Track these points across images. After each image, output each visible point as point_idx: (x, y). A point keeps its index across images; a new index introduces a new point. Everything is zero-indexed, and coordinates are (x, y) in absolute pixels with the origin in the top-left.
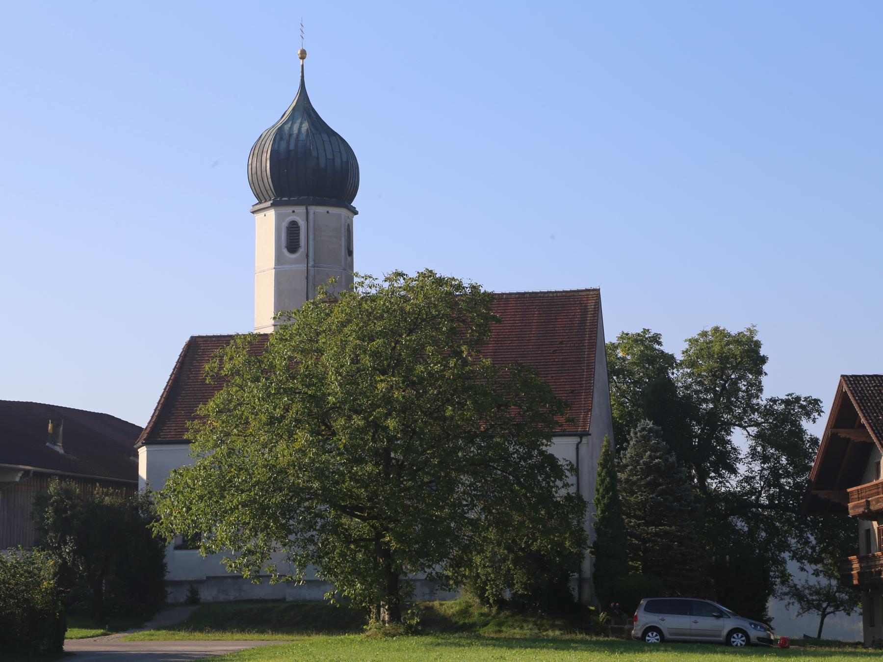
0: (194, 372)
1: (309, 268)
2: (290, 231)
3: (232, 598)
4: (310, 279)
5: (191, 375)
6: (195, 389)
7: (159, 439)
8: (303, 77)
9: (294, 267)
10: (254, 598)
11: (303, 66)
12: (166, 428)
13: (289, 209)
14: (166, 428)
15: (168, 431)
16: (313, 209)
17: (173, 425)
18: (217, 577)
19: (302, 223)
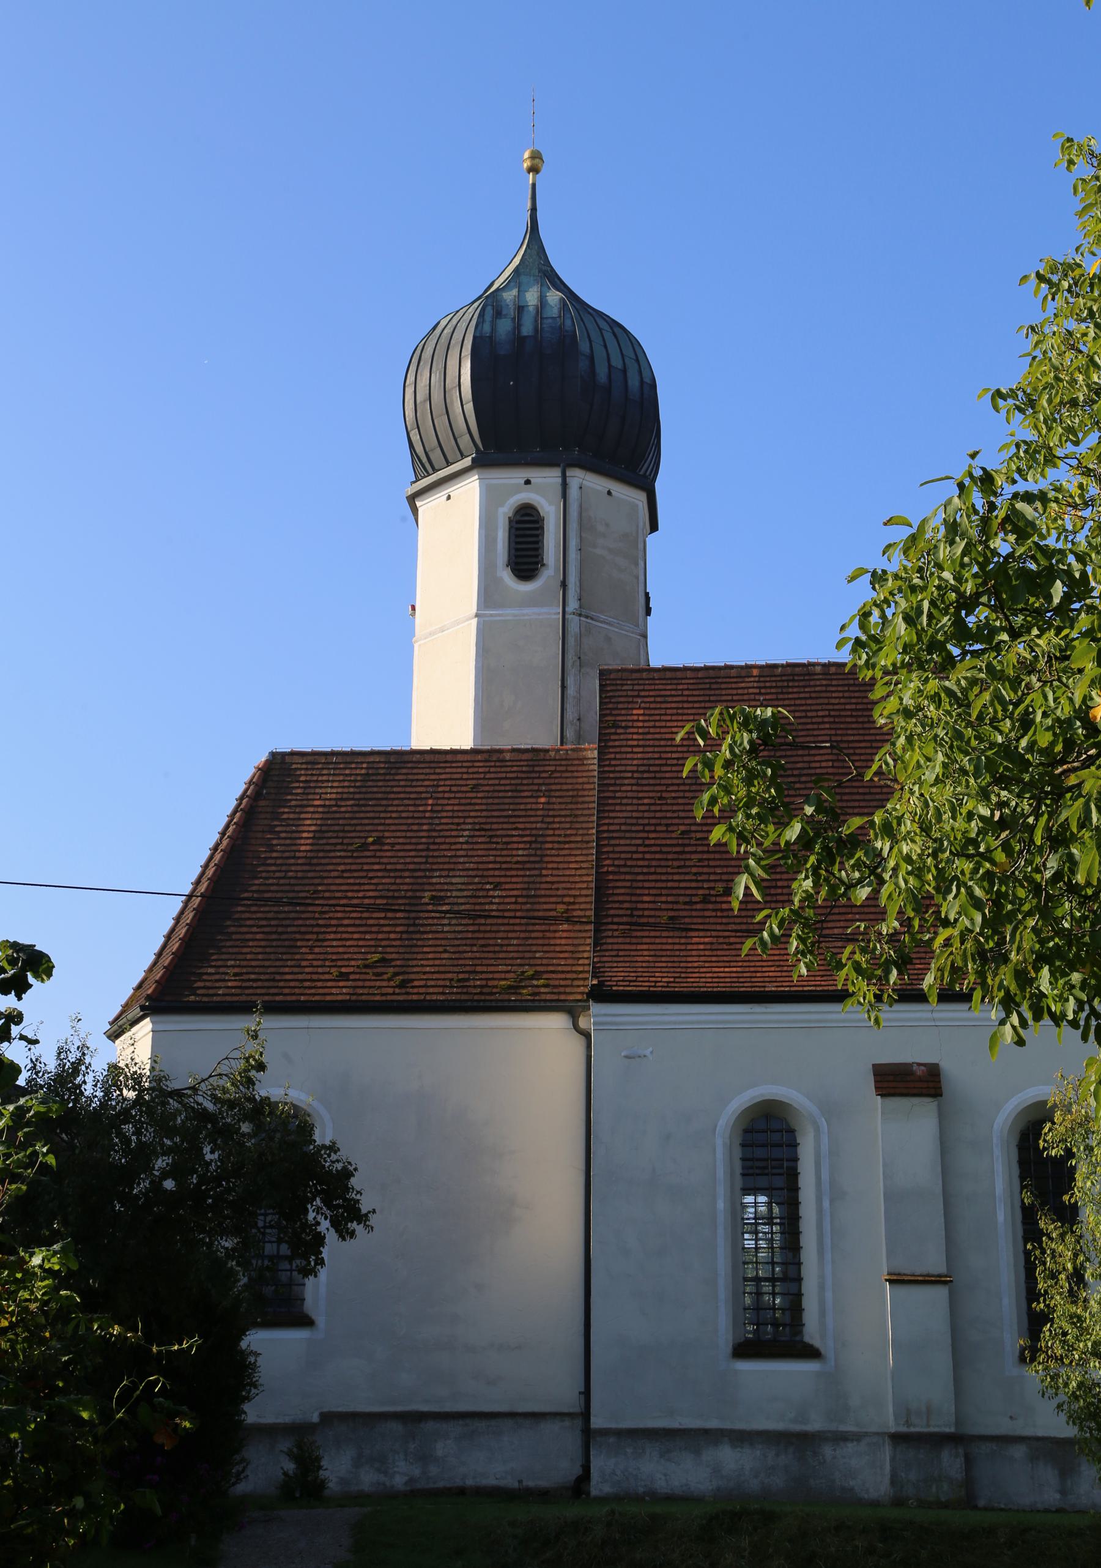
0: (283, 835)
1: (567, 616)
2: (517, 529)
3: (399, 1482)
4: (571, 641)
5: (275, 842)
6: (290, 874)
7: (192, 998)
8: (534, 209)
9: (531, 613)
10: (470, 1482)
11: (534, 186)
12: (210, 970)
13: (515, 476)
14: (210, 970)
15: (217, 977)
16: (578, 477)
17: (230, 963)
18: (353, 1416)
19: (550, 511)
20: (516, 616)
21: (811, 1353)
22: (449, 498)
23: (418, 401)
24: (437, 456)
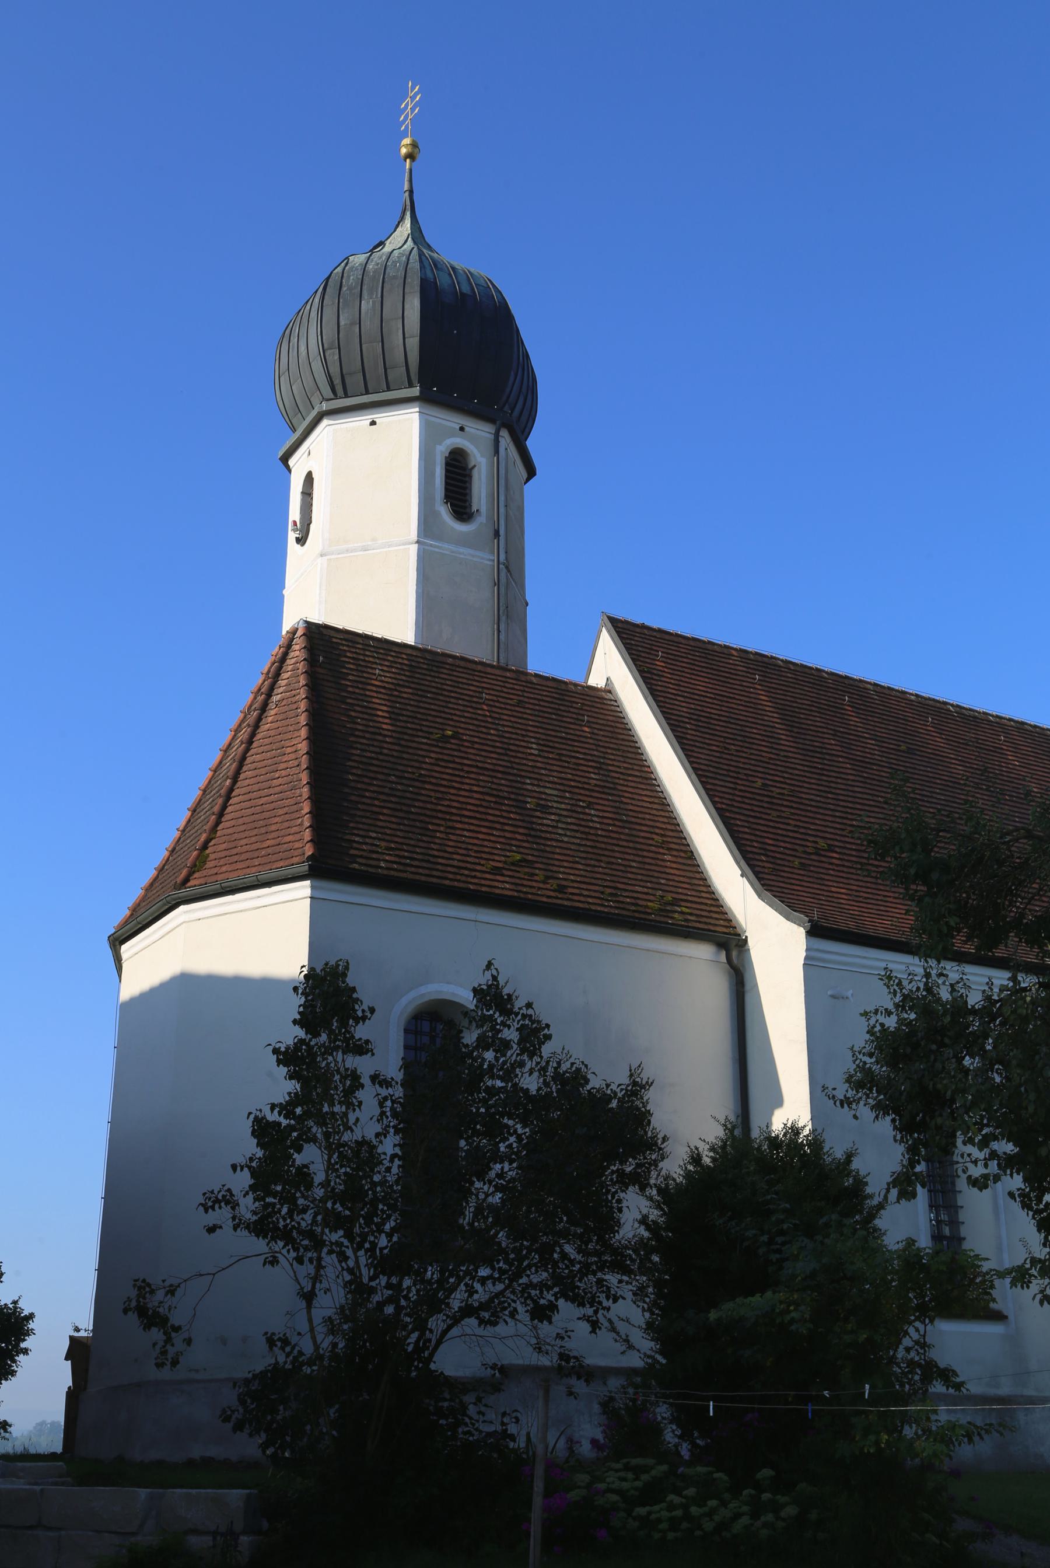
9: (465, 553)
11: (411, 170)
20: (453, 552)
21: (999, 1317)
22: (373, 423)
23: (342, 323)
24: (355, 381)
